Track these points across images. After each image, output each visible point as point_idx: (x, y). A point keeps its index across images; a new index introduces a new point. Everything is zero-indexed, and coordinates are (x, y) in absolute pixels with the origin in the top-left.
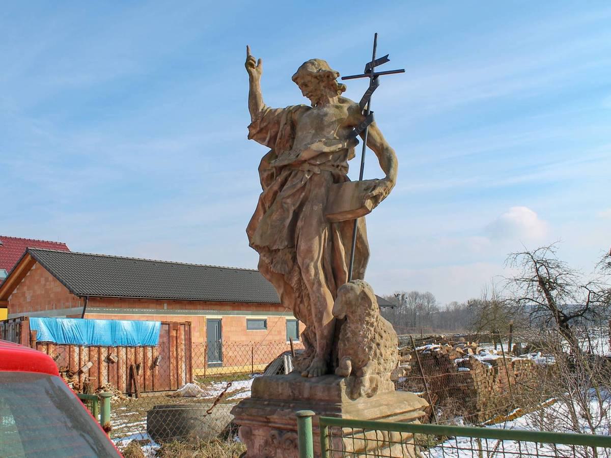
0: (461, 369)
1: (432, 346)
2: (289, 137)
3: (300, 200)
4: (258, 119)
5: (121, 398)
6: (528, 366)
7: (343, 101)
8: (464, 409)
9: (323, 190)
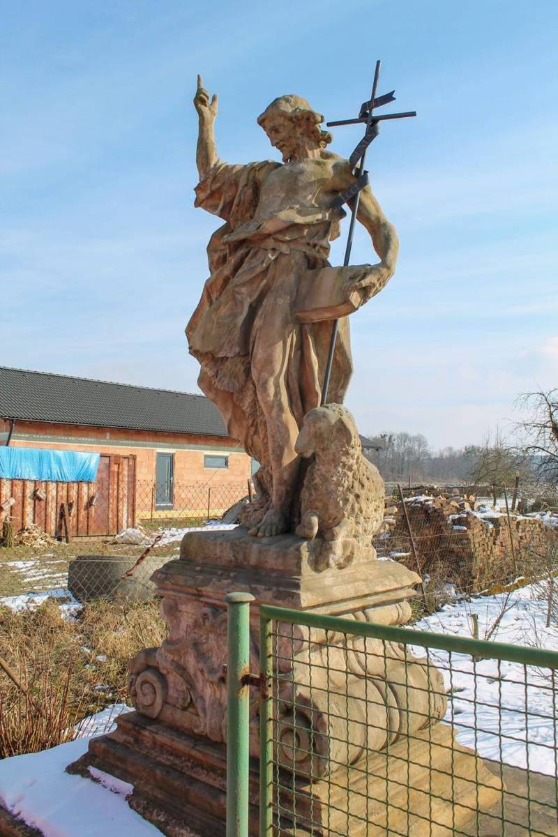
0: (456, 527)
1: (422, 498)
2: (249, 204)
3: (260, 289)
4: (208, 178)
5: (48, 543)
6: (535, 527)
7: (326, 156)
8: (457, 576)
9: (292, 277)
